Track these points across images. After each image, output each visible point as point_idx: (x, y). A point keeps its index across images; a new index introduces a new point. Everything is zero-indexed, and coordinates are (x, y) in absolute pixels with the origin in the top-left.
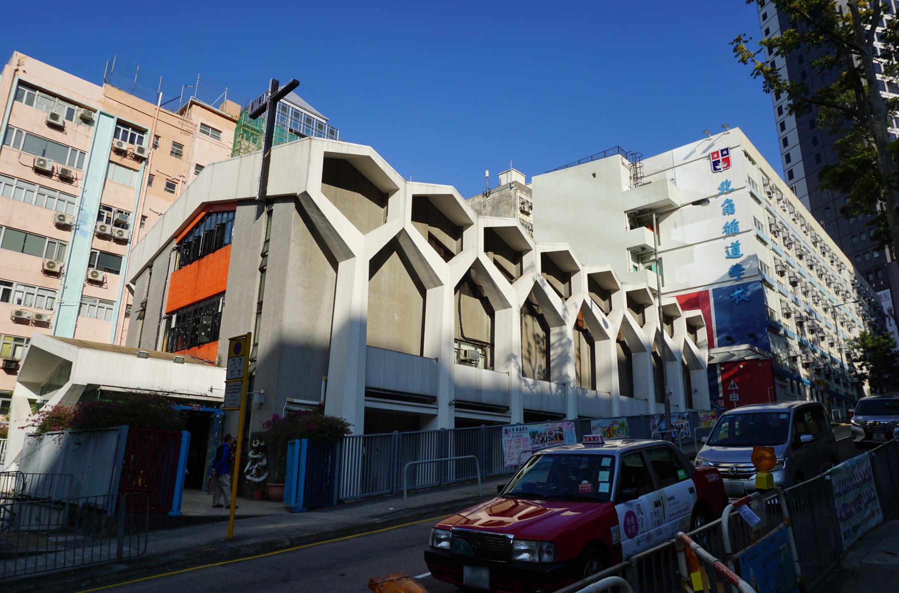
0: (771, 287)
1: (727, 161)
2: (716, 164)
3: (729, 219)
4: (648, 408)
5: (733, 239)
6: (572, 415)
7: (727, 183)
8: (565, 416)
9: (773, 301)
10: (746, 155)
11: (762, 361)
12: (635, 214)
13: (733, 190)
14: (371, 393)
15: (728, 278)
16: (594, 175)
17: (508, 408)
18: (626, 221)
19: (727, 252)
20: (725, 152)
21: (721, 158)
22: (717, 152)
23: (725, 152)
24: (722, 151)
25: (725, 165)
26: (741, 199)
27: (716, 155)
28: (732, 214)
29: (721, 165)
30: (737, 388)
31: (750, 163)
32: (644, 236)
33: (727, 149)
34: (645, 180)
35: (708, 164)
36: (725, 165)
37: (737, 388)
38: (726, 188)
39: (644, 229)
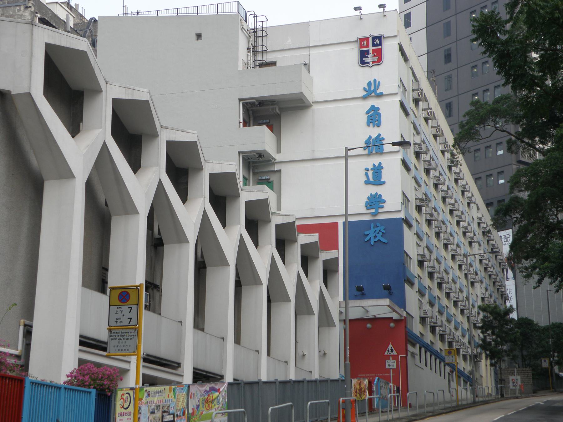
0: (410, 226)
1: (379, 54)
2: (363, 54)
3: (373, 132)
4: (287, 371)
5: (375, 160)
6: (229, 378)
7: (377, 84)
8: (222, 377)
9: (411, 245)
10: (401, 49)
11: (396, 321)
12: (253, 104)
13: (380, 95)
14: (81, 336)
15: (364, 210)
16: (199, 36)
17: (179, 365)
18: (238, 114)
19: (367, 175)
20: (377, 42)
21: (371, 48)
22: (367, 39)
23: (377, 42)
24: (374, 38)
25: (376, 59)
26: (389, 108)
27: (365, 43)
28: (379, 126)
29: (370, 58)
30: (395, 353)
31: (402, 59)
32: (260, 138)
33: (379, 38)
34: (268, 58)
35: (353, 53)
36: (376, 59)
37: (395, 353)
38: (372, 91)
39: (265, 128)
